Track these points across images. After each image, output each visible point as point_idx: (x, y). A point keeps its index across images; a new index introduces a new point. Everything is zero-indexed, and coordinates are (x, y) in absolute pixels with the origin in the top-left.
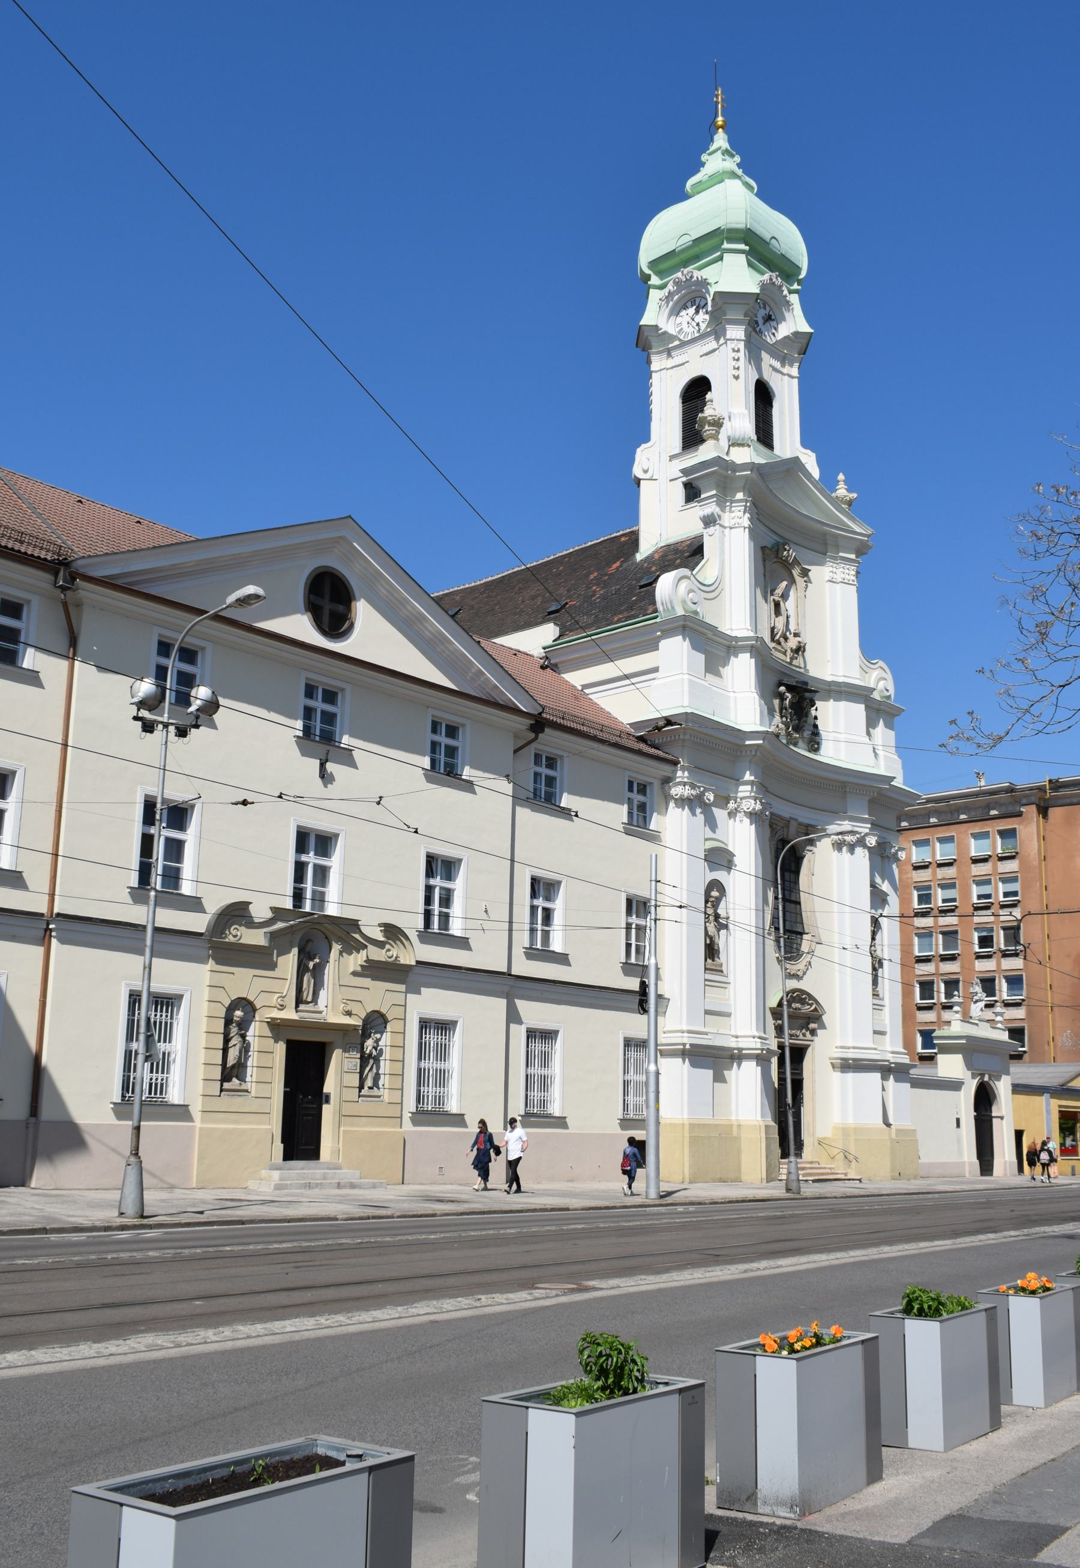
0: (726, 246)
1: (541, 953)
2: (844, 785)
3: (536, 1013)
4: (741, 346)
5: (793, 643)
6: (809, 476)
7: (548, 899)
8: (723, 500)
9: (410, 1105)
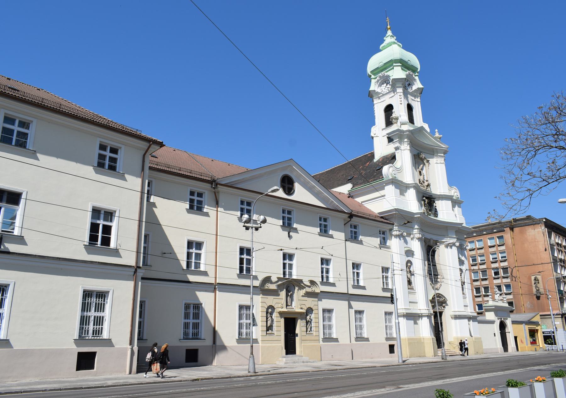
0: (394, 64)
1: (358, 287)
2: (447, 227)
3: (357, 305)
4: (402, 94)
5: (426, 183)
6: (426, 131)
7: (357, 269)
8: (401, 142)
9: (322, 336)
